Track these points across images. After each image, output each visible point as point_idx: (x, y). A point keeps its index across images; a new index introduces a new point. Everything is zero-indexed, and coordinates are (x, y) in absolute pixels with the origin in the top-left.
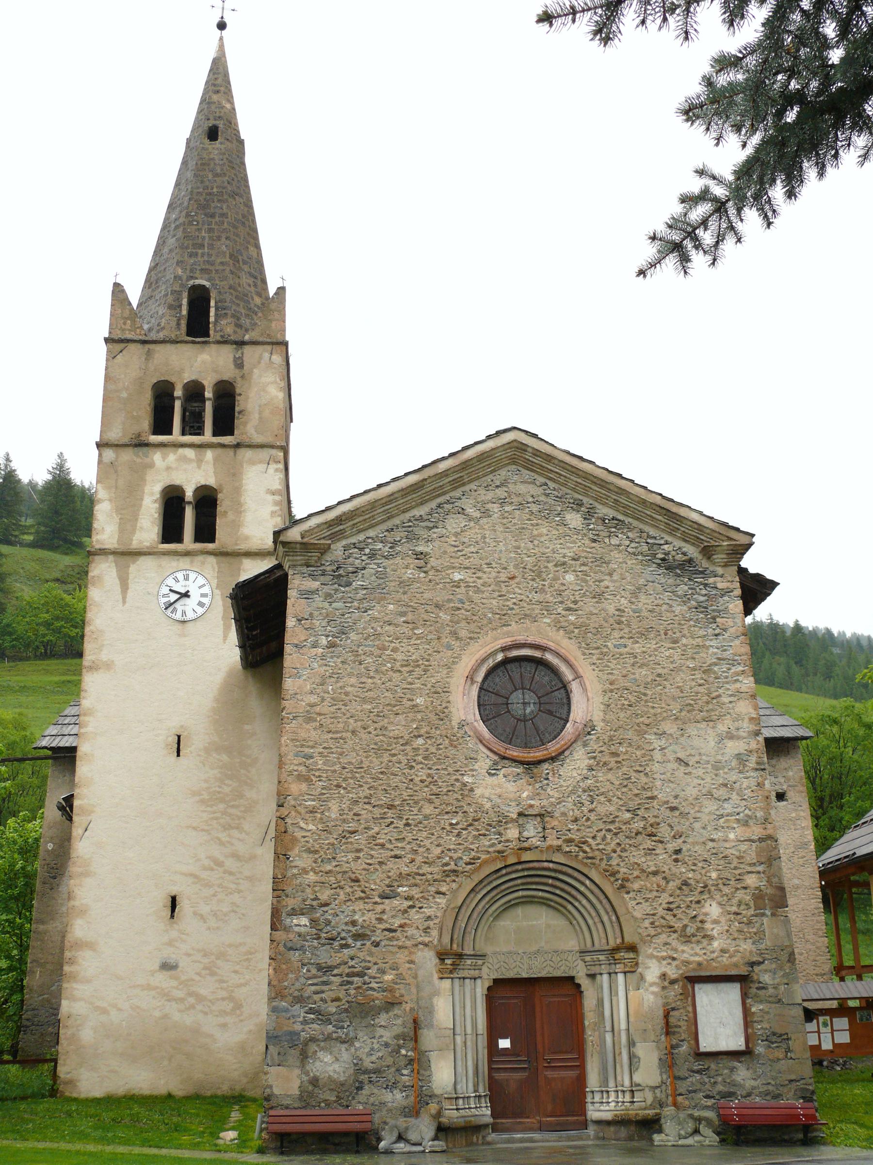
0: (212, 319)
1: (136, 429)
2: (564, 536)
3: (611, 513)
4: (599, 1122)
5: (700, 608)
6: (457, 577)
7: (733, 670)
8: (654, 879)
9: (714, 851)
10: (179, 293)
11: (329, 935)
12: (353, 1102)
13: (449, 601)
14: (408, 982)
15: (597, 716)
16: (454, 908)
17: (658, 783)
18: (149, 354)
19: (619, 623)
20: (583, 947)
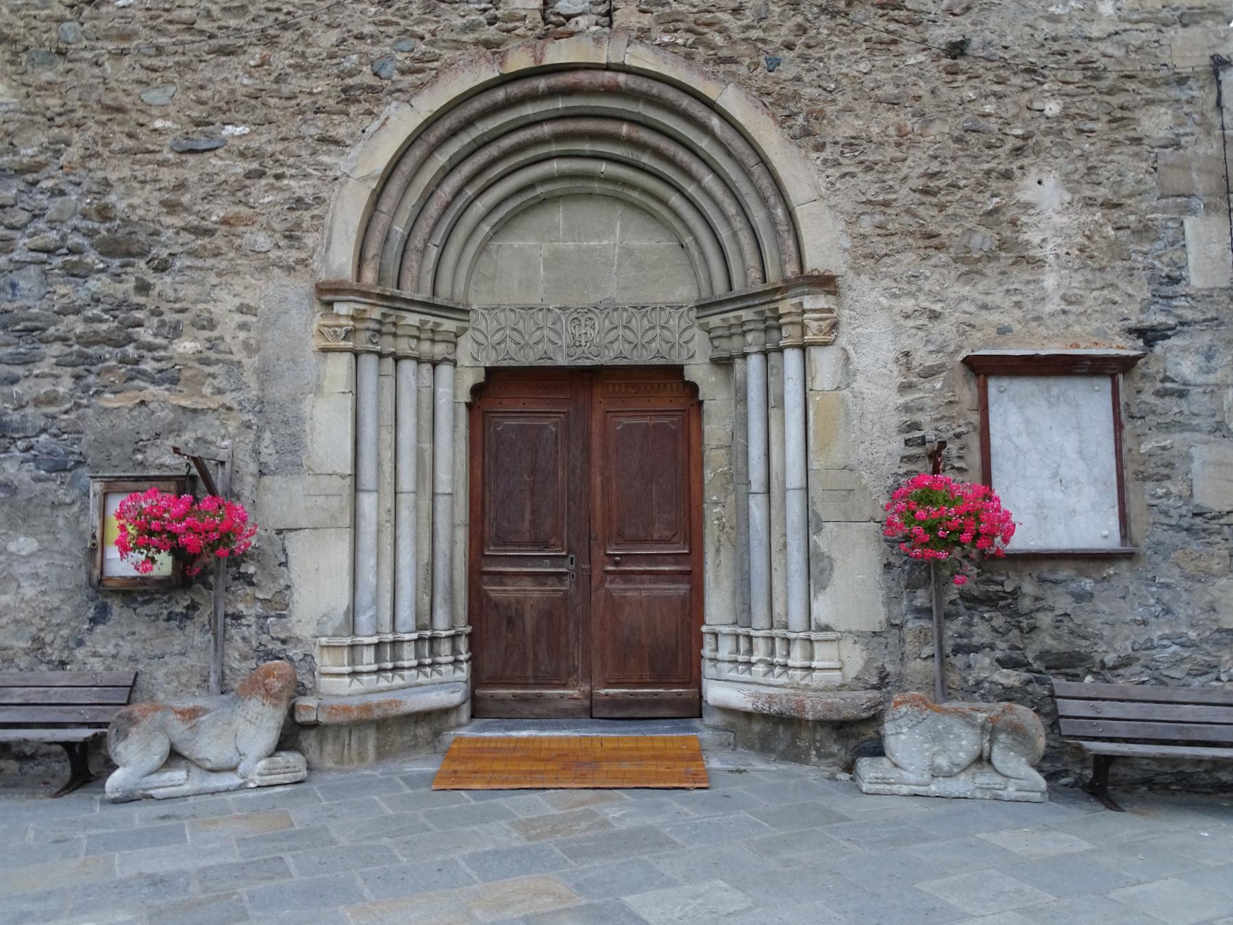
8: (890, 115)
9: (1056, 47)
11: (38, 241)
12: (80, 653)
14: (236, 358)
16: (364, 179)
20: (706, 294)
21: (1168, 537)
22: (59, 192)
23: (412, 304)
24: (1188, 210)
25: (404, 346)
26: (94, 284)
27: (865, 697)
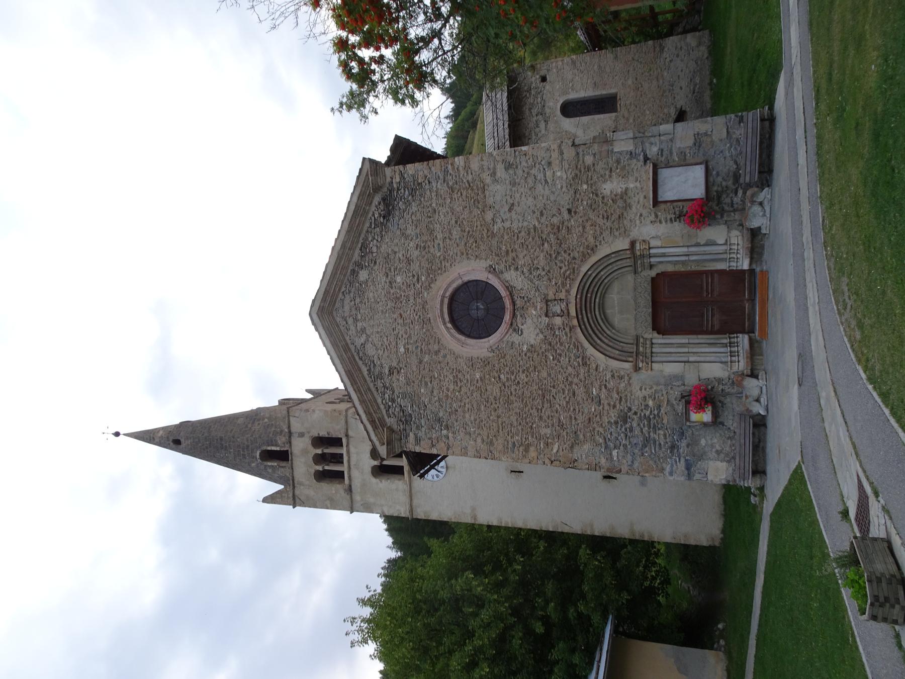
0: (278, 449)
1: (342, 492)
2: (375, 282)
3: (357, 251)
4: (751, 264)
5: (413, 192)
6: (402, 350)
7: (450, 171)
10: (266, 466)
11: (624, 438)
13: (417, 355)
15: (484, 264)
17: (525, 224)
18: (301, 484)
19: (425, 248)
21: (701, 152)
22: (611, 434)
23: (637, 349)
24: (612, 151)
25: (648, 351)
26: (635, 424)
27: (745, 231)
